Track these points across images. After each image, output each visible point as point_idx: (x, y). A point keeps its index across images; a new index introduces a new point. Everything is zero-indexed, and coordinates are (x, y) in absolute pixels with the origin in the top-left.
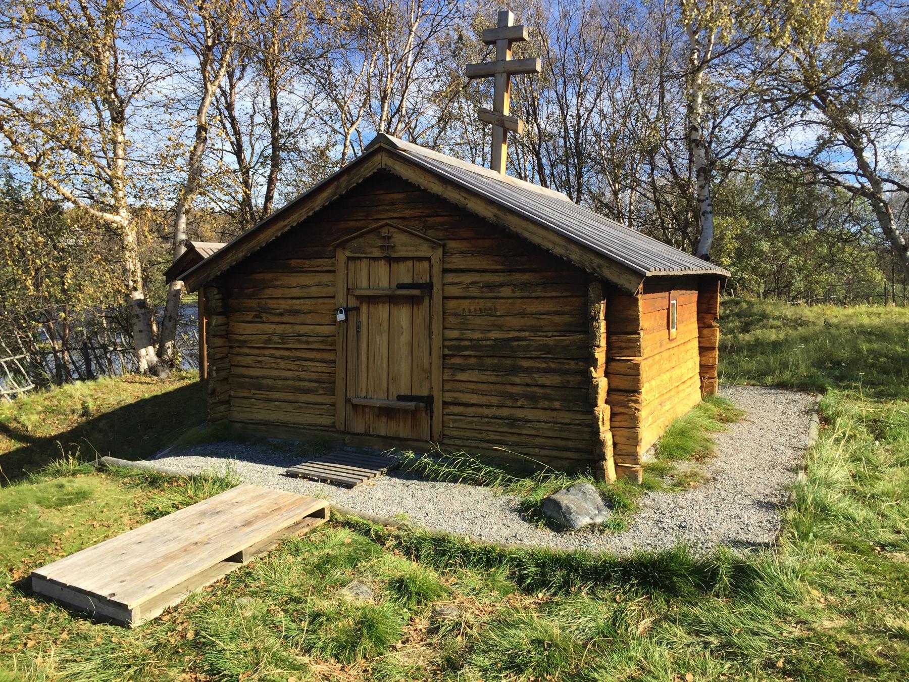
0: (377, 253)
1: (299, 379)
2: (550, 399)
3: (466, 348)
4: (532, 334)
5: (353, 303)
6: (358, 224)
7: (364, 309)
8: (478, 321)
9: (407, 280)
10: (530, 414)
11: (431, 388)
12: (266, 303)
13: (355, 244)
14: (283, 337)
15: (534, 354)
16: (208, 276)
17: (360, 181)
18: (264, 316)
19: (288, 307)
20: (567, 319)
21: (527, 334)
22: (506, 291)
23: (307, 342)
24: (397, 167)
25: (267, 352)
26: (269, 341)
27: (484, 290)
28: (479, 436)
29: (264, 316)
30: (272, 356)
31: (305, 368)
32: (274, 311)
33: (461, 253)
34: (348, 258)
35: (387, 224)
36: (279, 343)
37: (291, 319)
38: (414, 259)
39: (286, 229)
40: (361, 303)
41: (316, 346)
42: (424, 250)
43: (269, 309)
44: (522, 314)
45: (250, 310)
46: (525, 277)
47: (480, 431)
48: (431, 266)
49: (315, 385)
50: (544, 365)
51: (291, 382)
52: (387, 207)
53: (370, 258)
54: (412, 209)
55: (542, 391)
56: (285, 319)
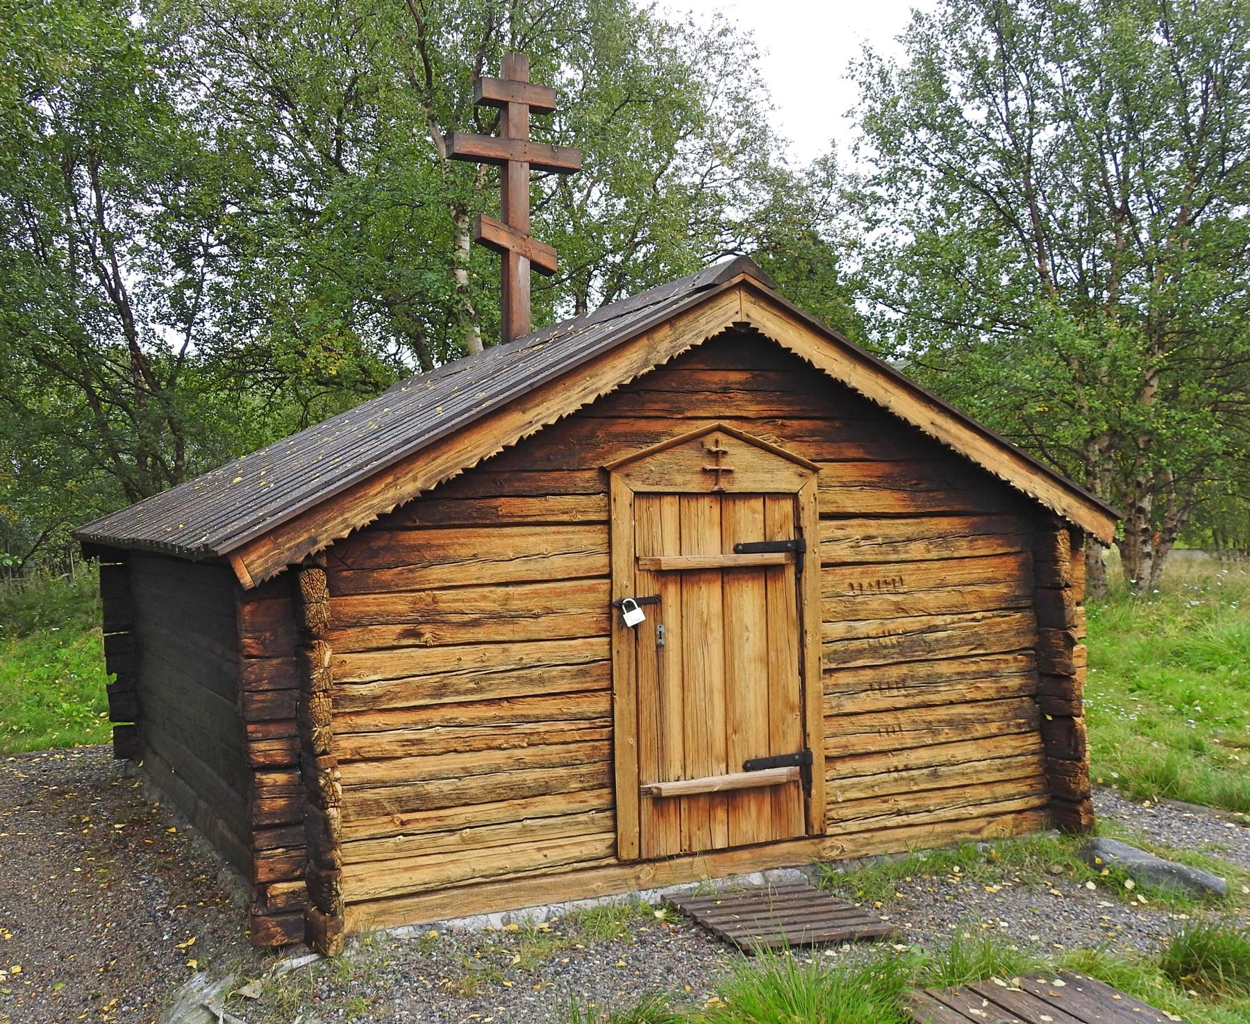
0: (696, 484)
1: (521, 765)
2: (985, 721)
3: (860, 653)
4: (956, 618)
5: (649, 588)
6: (657, 426)
7: (671, 595)
8: (875, 604)
9: (755, 537)
10: (959, 752)
11: (805, 734)
12: (435, 601)
13: (651, 464)
14: (484, 675)
15: (962, 651)
16: (314, 541)
17: (700, 342)
18: (427, 632)
19: (496, 607)
20: (1002, 589)
21: (948, 618)
22: (916, 550)
23: (541, 681)
24: (769, 324)
25: (436, 716)
26: (441, 690)
27: (884, 548)
28: (885, 806)
29: (427, 632)
30: (447, 724)
31: (535, 739)
32: (455, 618)
33: (844, 485)
34: (638, 495)
35: (720, 429)
36: (467, 692)
37: (505, 632)
38: (764, 495)
39: (532, 431)
40: (665, 586)
41: (564, 686)
42: (784, 478)
43: (439, 613)
44: (942, 585)
45: (387, 619)
46: (944, 524)
47: (883, 798)
48: (797, 510)
49: (561, 771)
50: (974, 668)
51: (502, 778)
52: (714, 397)
53: (681, 495)
54: (758, 403)
55: (972, 711)
56: (480, 634)
